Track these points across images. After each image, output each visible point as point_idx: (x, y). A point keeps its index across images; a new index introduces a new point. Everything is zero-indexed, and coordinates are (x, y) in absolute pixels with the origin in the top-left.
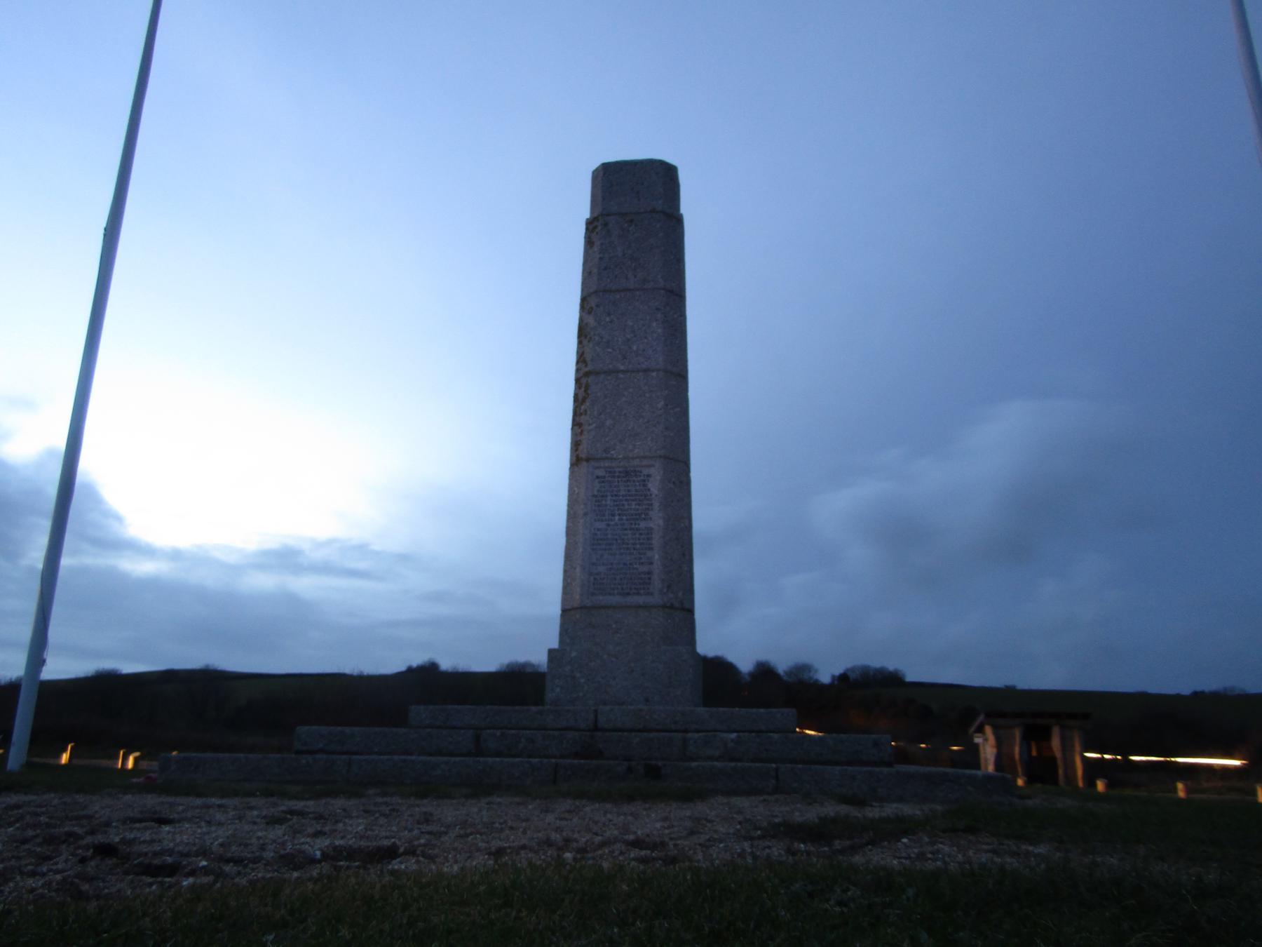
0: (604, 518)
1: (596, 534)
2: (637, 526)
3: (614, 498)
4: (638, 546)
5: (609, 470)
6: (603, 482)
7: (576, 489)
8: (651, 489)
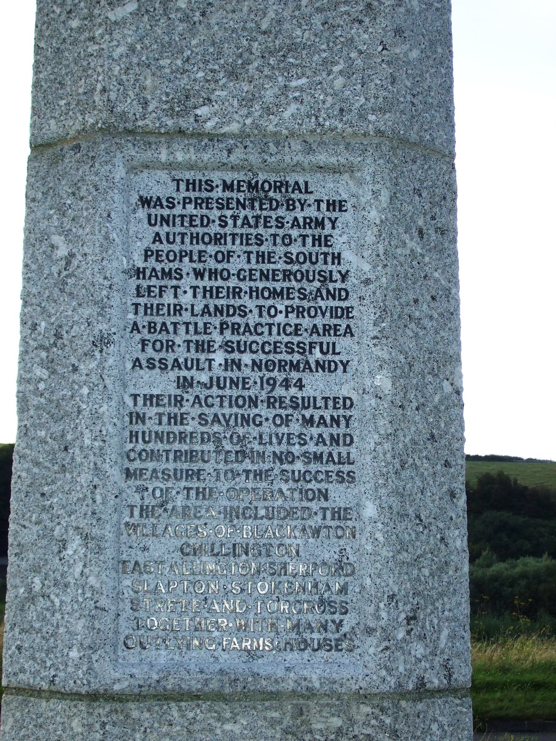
0: (171, 357)
1: (141, 418)
2: (293, 391)
3: (206, 282)
4: (299, 466)
5: (189, 175)
6: (165, 220)
7: (57, 239)
8: (347, 255)
